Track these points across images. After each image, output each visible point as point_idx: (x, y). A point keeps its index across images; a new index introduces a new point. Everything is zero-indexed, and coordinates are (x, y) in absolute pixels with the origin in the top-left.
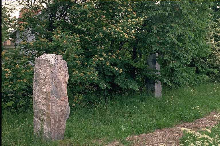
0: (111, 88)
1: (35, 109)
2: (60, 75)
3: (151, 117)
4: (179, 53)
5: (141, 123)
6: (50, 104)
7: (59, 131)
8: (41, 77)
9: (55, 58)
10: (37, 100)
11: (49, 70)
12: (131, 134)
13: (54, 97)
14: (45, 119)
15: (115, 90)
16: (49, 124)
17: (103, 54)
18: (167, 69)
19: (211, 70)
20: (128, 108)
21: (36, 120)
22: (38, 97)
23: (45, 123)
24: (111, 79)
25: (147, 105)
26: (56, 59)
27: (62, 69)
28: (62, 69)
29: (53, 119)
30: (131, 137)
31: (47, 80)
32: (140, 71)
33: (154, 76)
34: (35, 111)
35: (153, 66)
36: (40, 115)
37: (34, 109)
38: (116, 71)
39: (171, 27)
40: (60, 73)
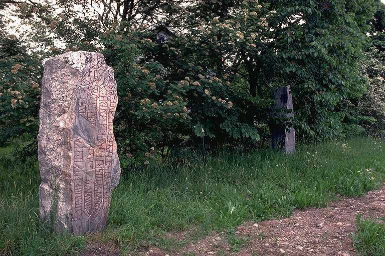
0: (215, 137)
2: (96, 94)
3: (282, 187)
5: (265, 196)
6: (71, 154)
7: (93, 211)
8: (54, 96)
10: (47, 145)
11: (71, 83)
12: (246, 218)
13: (82, 140)
14: (62, 186)
16: (69, 198)
17: (200, 76)
19: (365, 118)
20: (242, 170)
21: (43, 188)
22: (48, 140)
23: (61, 196)
25: (275, 164)
26: (89, 60)
28: (101, 83)
30: (245, 226)
33: (286, 120)
35: (282, 104)
36: (51, 177)
37: (40, 165)
39: (316, 34)
40: (95, 91)
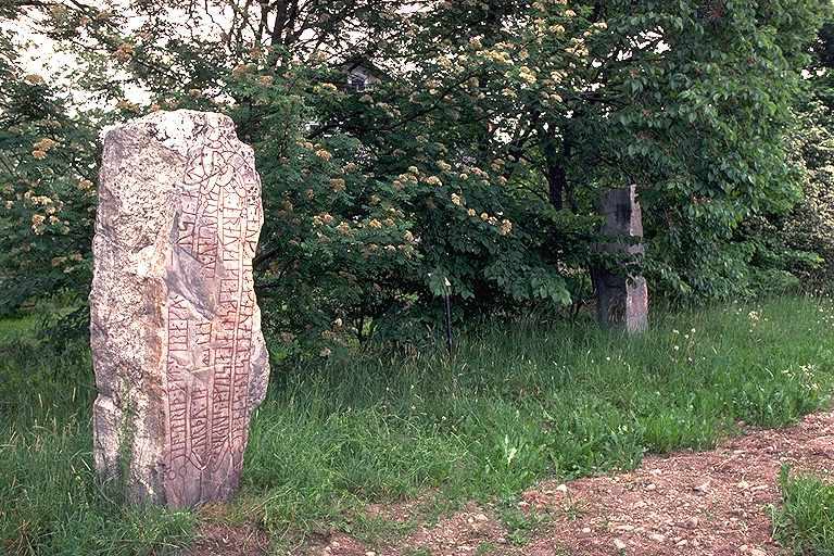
1: (99, 358)
3: (618, 404)
4: (724, 166)
5: (582, 426)
7: (209, 460)
8: (125, 209)
9: (197, 126)
11: (164, 178)
14: (142, 403)
15: (483, 303)
16: (158, 430)
17: (442, 164)
18: (666, 239)
19: (800, 255)
21: (101, 409)
22: (113, 302)
24: (471, 266)
26: (201, 129)
27: (226, 179)
28: (226, 179)
29: (178, 406)
31: (153, 222)
32: (574, 242)
34: (101, 367)
36: (118, 384)
38: (488, 230)
39: (693, 74)
